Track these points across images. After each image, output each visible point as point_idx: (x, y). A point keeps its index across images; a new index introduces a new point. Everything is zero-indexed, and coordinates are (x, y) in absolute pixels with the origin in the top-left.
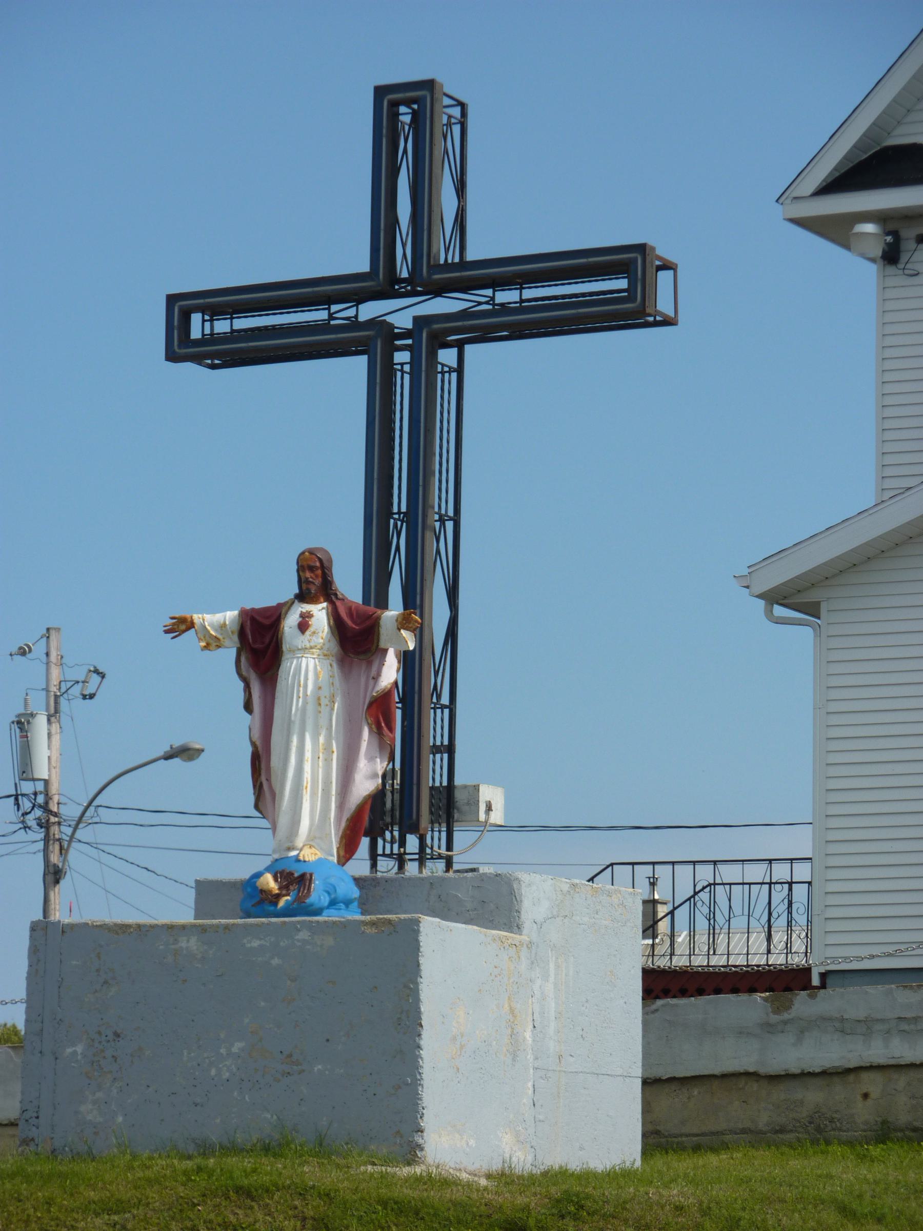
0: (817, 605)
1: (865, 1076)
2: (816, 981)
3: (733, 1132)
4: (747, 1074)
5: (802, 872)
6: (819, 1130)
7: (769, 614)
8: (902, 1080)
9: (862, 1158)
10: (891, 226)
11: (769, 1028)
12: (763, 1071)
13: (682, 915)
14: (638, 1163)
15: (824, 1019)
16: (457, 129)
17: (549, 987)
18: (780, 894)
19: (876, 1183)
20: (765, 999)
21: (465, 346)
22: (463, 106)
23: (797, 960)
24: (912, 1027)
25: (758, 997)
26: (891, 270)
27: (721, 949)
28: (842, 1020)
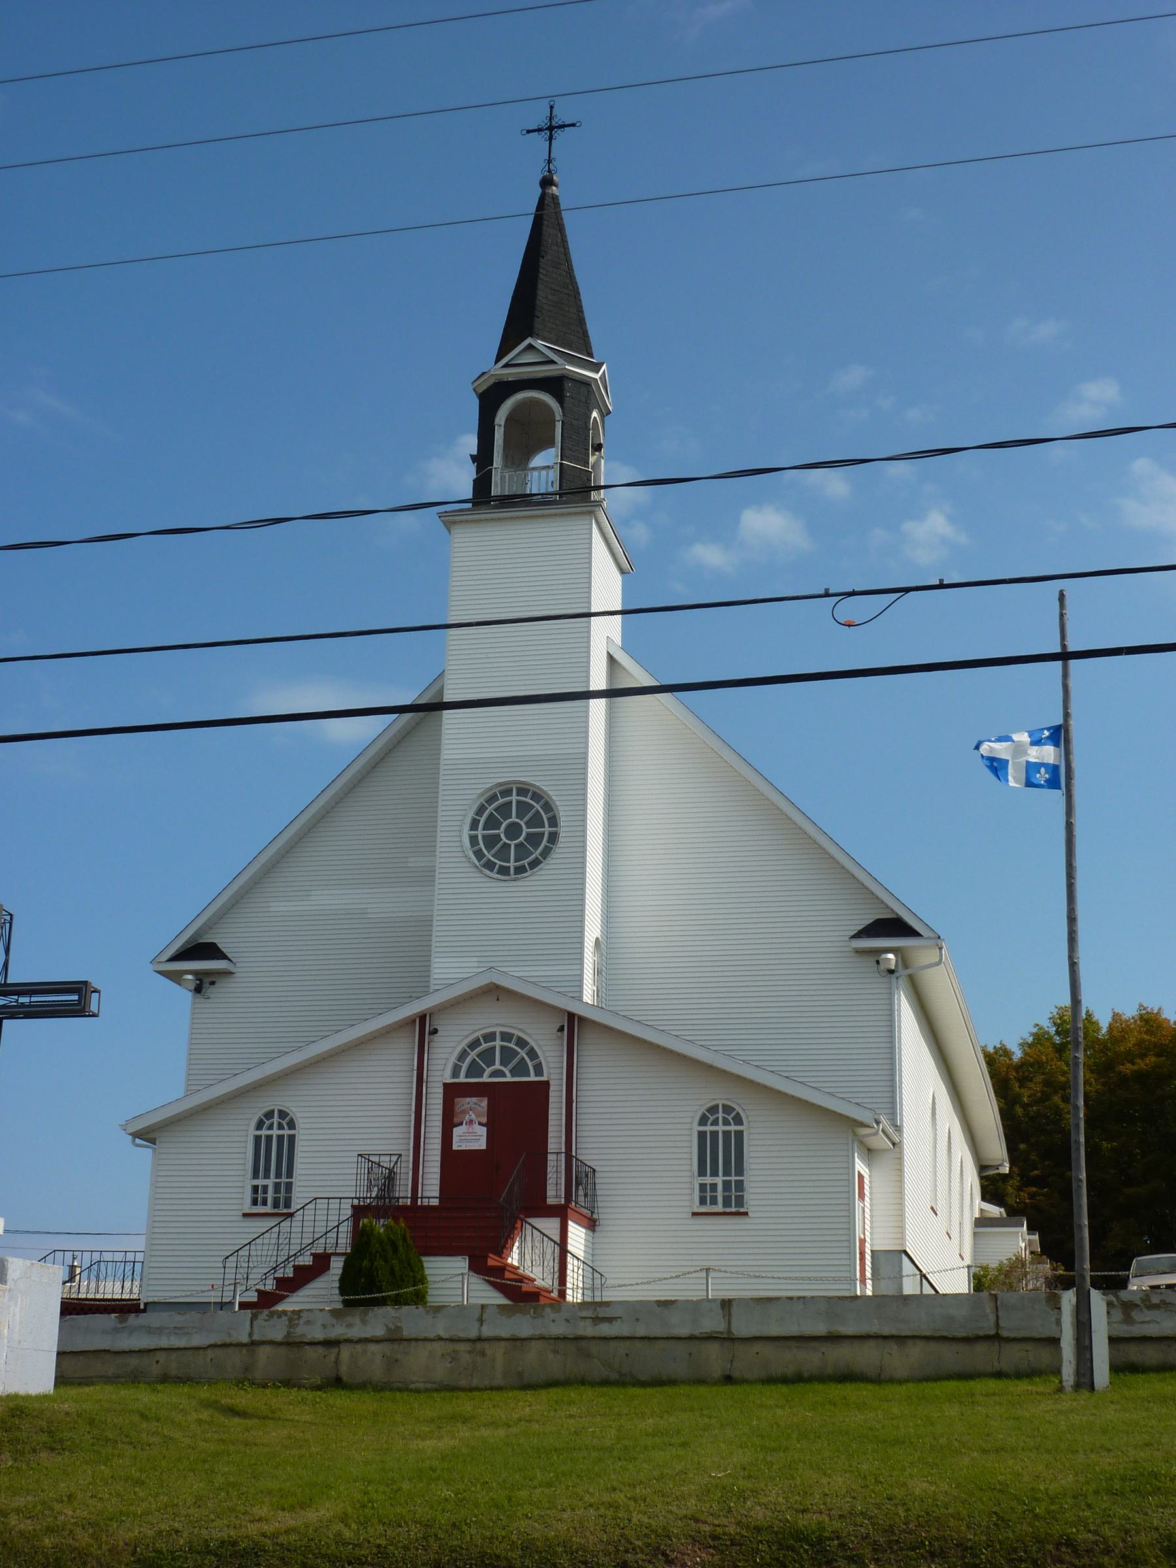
0: (155, 1139)
1: (158, 1353)
2: (142, 1307)
3: (97, 1377)
4: (105, 1350)
5: (140, 1257)
6: (136, 1377)
7: (133, 1141)
8: (174, 1356)
9: (154, 1390)
10: (200, 977)
11: (116, 1330)
12: (112, 1350)
13: (85, 1274)
14: (52, 1392)
15: (141, 1327)
16: (8, 925)
17: (17, 1310)
18: (129, 1267)
19: (158, 1403)
20: (116, 1317)
21: (471, 497)
22: (11, 915)
23: (135, 1297)
24: (180, 1331)
25: (113, 1315)
26: (198, 995)
27: (101, 1290)
28: (149, 1327)
